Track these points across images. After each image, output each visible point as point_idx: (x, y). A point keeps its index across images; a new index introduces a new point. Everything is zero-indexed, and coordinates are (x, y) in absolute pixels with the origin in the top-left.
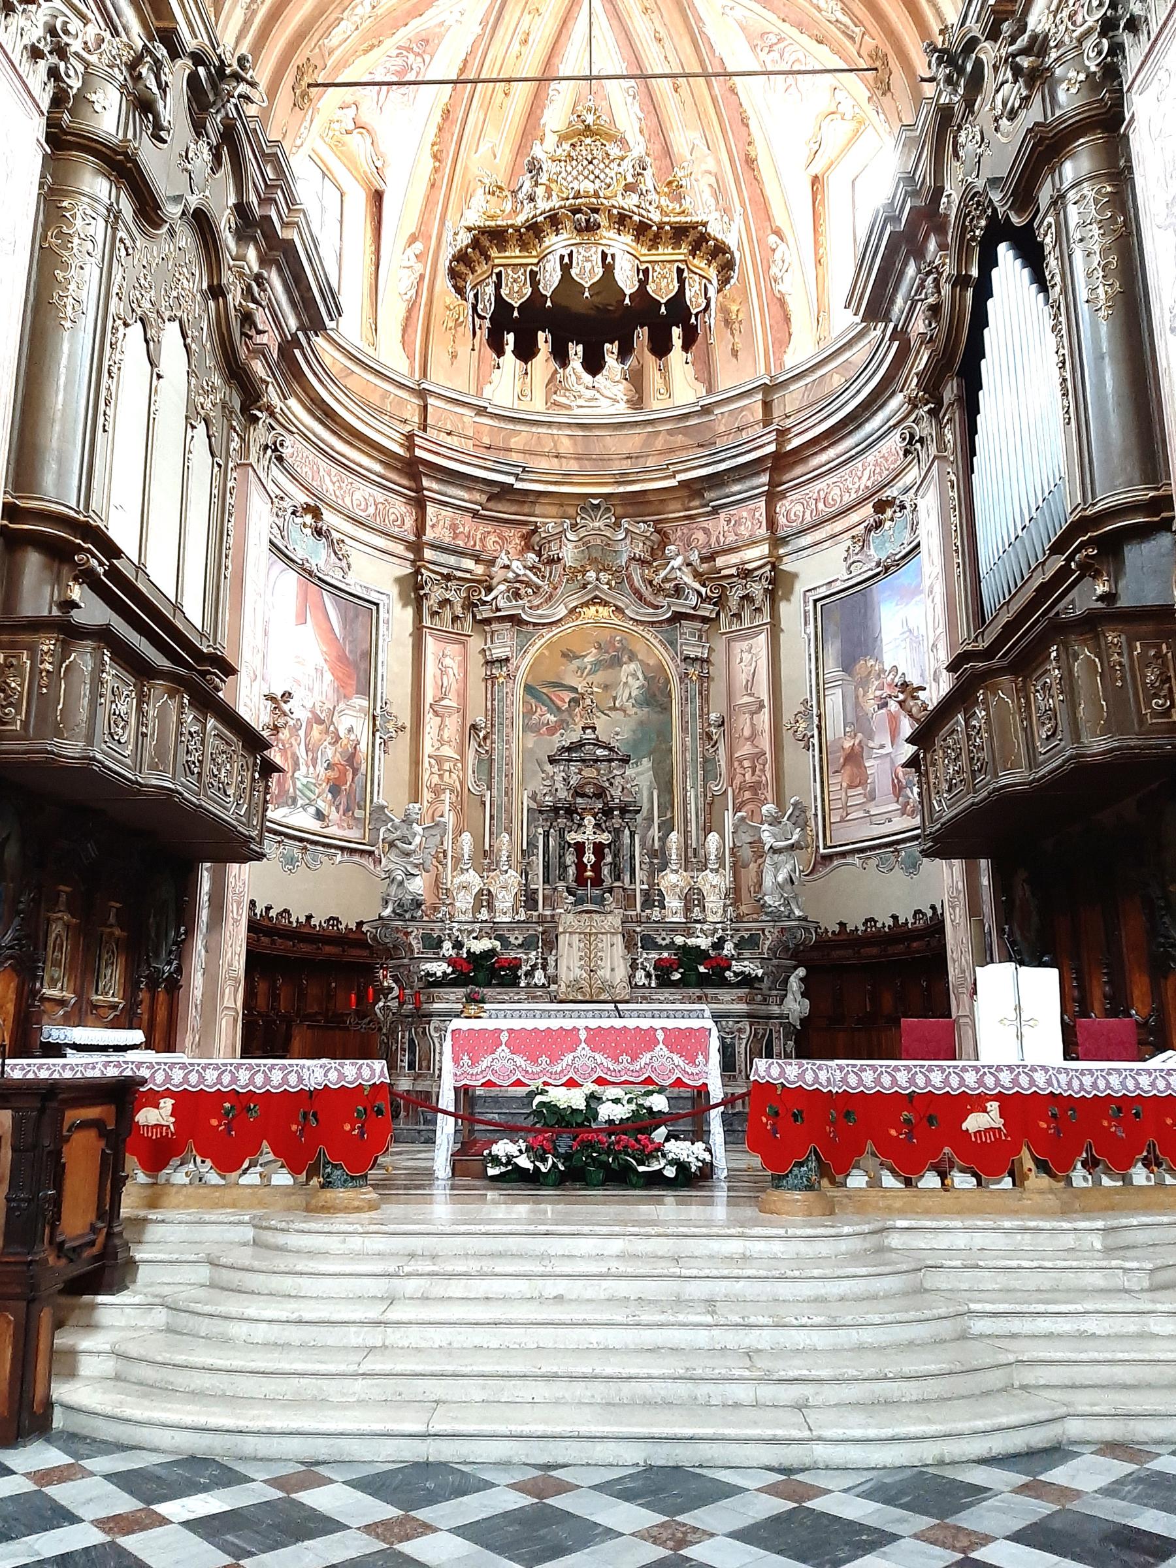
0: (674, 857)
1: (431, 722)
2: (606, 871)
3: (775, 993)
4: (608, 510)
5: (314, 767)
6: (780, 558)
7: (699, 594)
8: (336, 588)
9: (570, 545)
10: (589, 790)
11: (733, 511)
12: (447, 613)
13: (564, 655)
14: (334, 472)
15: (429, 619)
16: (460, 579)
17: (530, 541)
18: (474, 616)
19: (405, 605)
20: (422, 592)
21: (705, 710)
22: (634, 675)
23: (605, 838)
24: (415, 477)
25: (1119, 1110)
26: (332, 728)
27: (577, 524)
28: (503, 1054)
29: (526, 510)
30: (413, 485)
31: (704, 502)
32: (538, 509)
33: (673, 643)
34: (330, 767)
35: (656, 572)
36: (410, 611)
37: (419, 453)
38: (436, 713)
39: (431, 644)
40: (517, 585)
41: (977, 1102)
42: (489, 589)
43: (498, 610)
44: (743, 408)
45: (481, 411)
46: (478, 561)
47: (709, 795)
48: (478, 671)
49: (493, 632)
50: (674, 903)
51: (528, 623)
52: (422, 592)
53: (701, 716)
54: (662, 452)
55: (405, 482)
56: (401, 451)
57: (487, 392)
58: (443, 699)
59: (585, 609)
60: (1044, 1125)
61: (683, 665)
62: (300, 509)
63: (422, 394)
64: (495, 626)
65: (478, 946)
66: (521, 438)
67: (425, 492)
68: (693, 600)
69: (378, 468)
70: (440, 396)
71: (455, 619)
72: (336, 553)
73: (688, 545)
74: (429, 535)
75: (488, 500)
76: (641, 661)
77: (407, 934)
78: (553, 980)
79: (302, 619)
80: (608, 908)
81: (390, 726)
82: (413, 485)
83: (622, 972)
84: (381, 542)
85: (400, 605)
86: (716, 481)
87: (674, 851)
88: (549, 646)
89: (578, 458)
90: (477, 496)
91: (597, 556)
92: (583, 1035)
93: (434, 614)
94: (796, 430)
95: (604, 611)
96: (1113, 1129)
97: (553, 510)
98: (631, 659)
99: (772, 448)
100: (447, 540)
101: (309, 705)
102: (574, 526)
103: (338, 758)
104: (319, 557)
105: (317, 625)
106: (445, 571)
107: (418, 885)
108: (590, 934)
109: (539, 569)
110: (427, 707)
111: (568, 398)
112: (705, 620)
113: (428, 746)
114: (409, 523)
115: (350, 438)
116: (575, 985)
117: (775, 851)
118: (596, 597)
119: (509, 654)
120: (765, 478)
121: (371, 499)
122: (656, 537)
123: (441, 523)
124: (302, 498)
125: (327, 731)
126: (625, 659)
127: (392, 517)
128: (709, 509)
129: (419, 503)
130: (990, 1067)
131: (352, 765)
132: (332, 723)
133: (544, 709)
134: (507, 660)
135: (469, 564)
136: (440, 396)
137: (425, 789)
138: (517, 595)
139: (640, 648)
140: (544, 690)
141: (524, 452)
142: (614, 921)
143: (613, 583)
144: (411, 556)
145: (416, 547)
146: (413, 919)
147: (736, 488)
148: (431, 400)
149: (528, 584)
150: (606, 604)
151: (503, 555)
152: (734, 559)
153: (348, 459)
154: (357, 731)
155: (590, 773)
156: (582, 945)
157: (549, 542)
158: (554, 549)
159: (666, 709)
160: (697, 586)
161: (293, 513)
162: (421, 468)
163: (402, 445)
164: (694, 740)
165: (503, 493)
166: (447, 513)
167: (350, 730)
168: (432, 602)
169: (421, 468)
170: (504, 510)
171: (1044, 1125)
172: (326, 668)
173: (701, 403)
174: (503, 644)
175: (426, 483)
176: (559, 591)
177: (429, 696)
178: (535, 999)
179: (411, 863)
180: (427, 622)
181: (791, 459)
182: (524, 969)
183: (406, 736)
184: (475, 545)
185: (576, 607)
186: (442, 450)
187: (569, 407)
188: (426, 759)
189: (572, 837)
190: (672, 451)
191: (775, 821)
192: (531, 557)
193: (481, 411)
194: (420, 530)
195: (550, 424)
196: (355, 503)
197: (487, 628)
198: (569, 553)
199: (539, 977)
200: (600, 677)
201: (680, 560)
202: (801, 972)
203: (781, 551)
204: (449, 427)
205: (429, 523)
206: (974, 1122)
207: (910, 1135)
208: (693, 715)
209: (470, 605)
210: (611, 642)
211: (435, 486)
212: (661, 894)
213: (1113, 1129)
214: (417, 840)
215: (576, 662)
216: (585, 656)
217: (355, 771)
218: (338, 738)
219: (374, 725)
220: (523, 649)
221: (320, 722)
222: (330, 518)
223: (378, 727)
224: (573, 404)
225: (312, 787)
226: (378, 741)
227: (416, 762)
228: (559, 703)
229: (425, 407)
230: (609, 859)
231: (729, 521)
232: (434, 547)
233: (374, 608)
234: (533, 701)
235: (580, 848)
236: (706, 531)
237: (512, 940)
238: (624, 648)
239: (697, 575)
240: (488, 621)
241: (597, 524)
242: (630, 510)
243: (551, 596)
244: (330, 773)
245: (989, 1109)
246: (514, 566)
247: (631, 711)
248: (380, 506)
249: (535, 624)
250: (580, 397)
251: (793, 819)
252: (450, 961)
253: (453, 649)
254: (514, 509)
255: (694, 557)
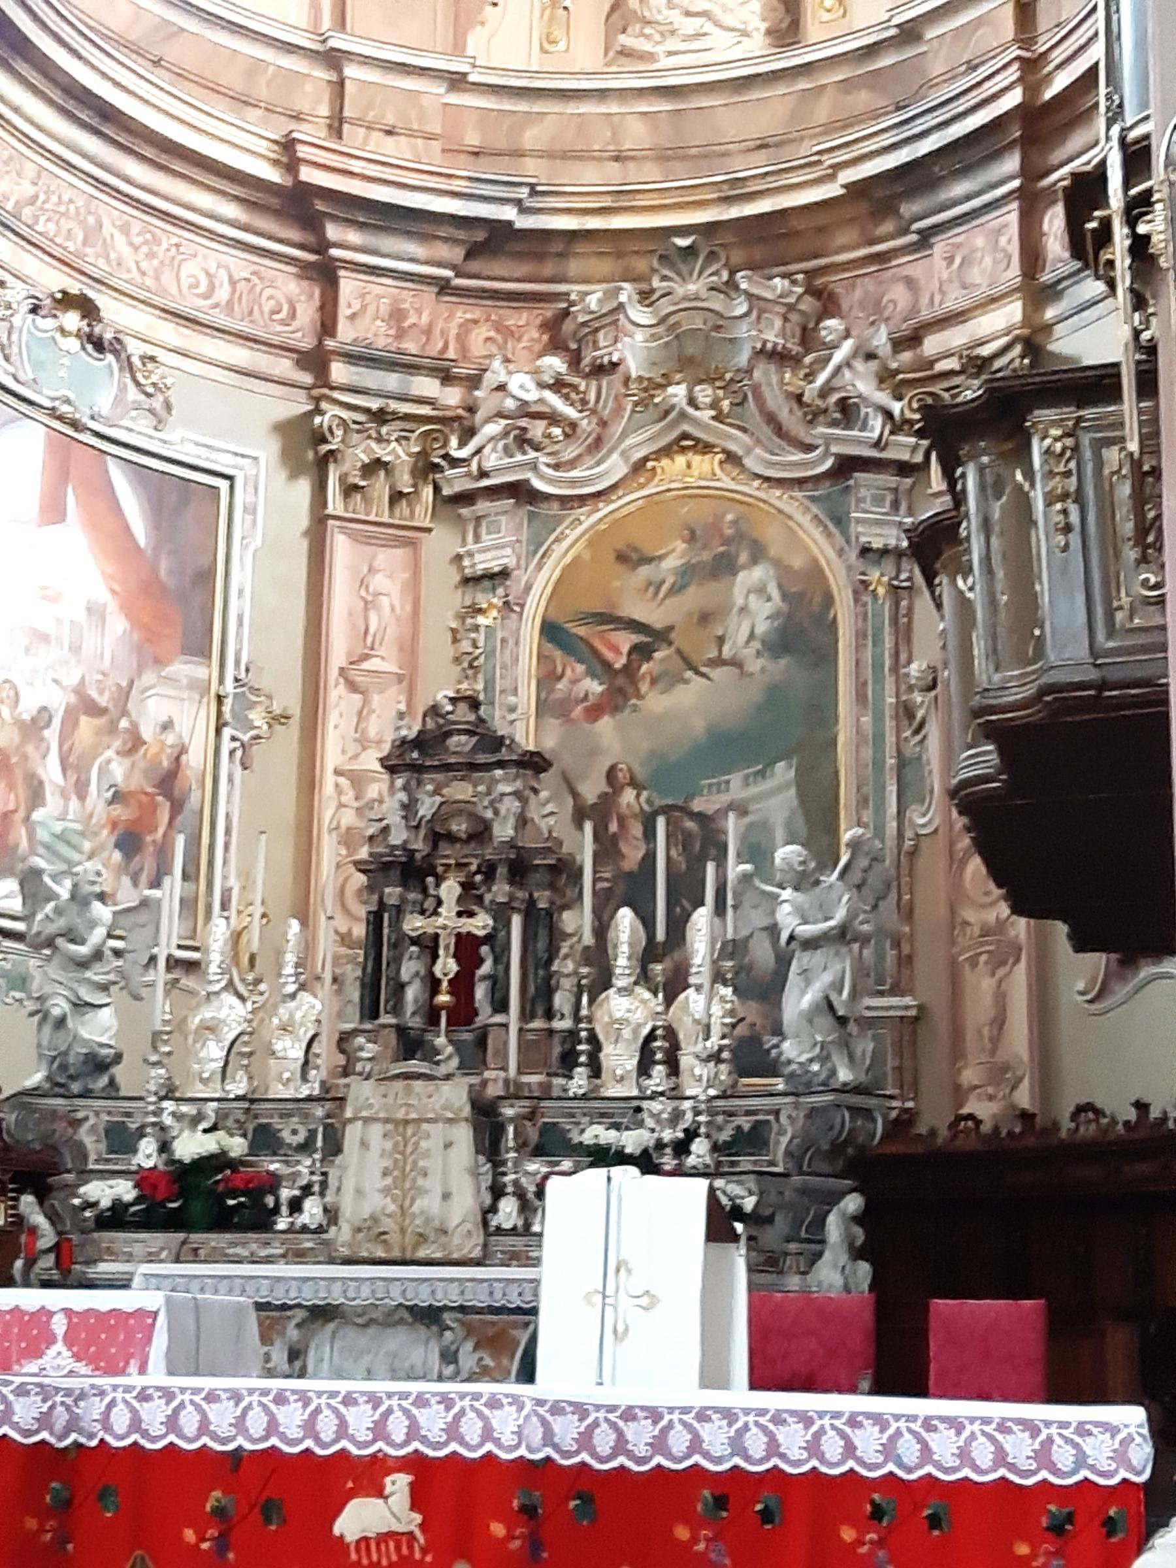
0: (622, 961)
1: (339, 706)
2: (481, 992)
3: (793, 1247)
4: (712, 256)
5: (82, 797)
6: (1048, 328)
7: (888, 415)
8: (126, 446)
9: (639, 336)
10: (459, 827)
11: (957, 235)
12: (380, 487)
13: (622, 558)
14: (136, 227)
15: (339, 498)
16: (407, 417)
17: (560, 334)
18: (437, 489)
19: (293, 475)
20: (325, 448)
21: (903, 657)
22: (761, 590)
23: (480, 924)
24: (311, 222)
25: (720, 1502)
26: (124, 723)
27: (653, 291)
28: (59, 1361)
29: (548, 269)
30: (311, 239)
31: (904, 224)
32: (574, 267)
33: (840, 521)
34: (118, 797)
35: (810, 377)
36: (303, 487)
37: (307, 175)
38: (353, 687)
39: (341, 547)
40: (523, 422)
41: (366, 1475)
42: (468, 433)
43: (483, 474)
44: (979, 21)
45: (457, 81)
46: (447, 378)
47: (909, 834)
48: (444, 601)
49: (478, 519)
50: (620, 1058)
51: (548, 497)
52: (325, 448)
53: (895, 669)
54: (829, 128)
55: (294, 235)
56: (273, 175)
57: (475, 42)
58: (365, 657)
59: (665, 462)
60: (498, 1529)
61: (859, 565)
62: (48, 302)
63: (333, 59)
64: (482, 506)
65: (191, 1145)
66: (545, 126)
67: (334, 252)
68: (877, 424)
69: (231, 210)
70: (368, 61)
71: (396, 497)
72: (138, 384)
73: (877, 310)
74: (346, 333)
75: (469, 255)
76: (777, 563)
77: (77, 1123)
78: (332, 1214)
79: (53, 511)
80: (443, 1070)
81: (257, 717)
82: (311, 239)
83: (465, 1201)
84: (240, 355)
85: (282, 475)
86: (916, 177)
87: (625, 948)
88: (595, 540)
89: (664, 156)
90: (444, 251)
91: (691, 353)
92: (59, 1325)
93: (349, 490)
94: (1058, 56)
95: (703, 464)
96: (701, 1546)
97: (605, 266)
98: (758, 554)
99: (1014, 98)
100: (381, 342)
101: (72, 680)
102: (646, 297)
103: (137, 782)
104: (100, 392)
105: (92, 523)
106: (374, 404)
107: (100, 1029)
108: (406, 1122)
109: (574, 387)
110: (334, 673)
111: (647, 37)
112: (903, 468)
113: (333, 753)
114: (308, 313)
115: (163, 159)
116: (371, 1228)
117: (811, 944)
118: (685, 436)
119: (511, 562)
120: (1012, 163)
121: (223, 275)
122: (809, 304)
123: (371, 309)
124: (55, 280)
125: (112, 729)
126: (743, 558)
127: (268, 306)
128: (914, 237)
129: (324, 273)
130: (685, 1410)
131: (169, 796)
132: (125, 713)
133: (580, 668)
134: (504, 574)
135: (427, 386)
136: (368, 61)
137: (326, 838)
138: (523, 441)
139: (773, 536)
140: (581, 631)
141: (549, 155)
142: (454, 1095)
143: (725, 405)
144: (307, 379)
145: (315, 361)
146: (86, 1094)
147: (960, 188)
148: (350, 71)
149: (553, 418)
150: (705, 448)
151: (497, 364)
152: (956, 337)
153: (166, 198)
154: (183, 726)
155: (461, 791)
156: (389, 1145)
157: (597, 330)
158: (604, 349)
159: (825, 658)
160: (883, 397)
161: (34, 310)
162: (320, 206)
163: (276, 162)
164: (878, 719)
165: (491, 240)
166: (384, 289)
167: (167, 726)
168: (346, 468)
169: (320, 206)
170: (504, 275)
171: (498, 1529)
172: (112, 606)
173: (895, 21)
174: (498, 542)
175: (333, 232)
176: (617, 429)
177: (338, 651)
178: (300, 1256)
179: (88, 981)
180: (335, 503)
181: (1062, 117)
182: (286, 1193)
183: (290, 735)
184: (446, 346)
185: (646, 459)
186: (357, 166)
187: (650, 57)
188: (329, 780)
189: (414, 924)
190: (847, 124)
191: (803, 881)
192: (555, 364)
193: (457, 81)
194: (327, 326)
195: (602, 94)
196: (185, 282)
197: (464, 511)
198: (633, 351)
199: (312, 1212)
200: (694, 598)
201: (847, 346)
202: (853, 1203)
203: (1050, 313)
204: (390, 119)
205: (343, 311)
206: (358, 1519)
207: (222, 1543)
208: (878, 666)
209: (425, 468)
210: (715, 527)
211: (353, 237)
212: (593, 1040)
213: (701, 1546)
214: (99, 934)
215: (644, 571)
216: (661, 558)
217: (177, 806)
218: (135, 743)
219: (219, 714)
220: (536, 546)
221: (93, 709)
222: (116, 313)
223: (227, 716)
224: (659, 49)
225: (75, 839)
226: (226, 746)
227: (309, 783)
228: (609, 655)
229: (341, 83)
230: (486, 968)
231: (950, 260)
232: (352, 358)
233: (223, 485)
234: (558, 654)
235: (429, 946)
236: (910, 282)
237: (286, 1135)
238: (740, 537)
239: (885, 377)
240: (466, 498)
241: (692, 287)
242: (758, 254)
243: (598, 442)
244: (118, 811)
245: (388, 1489)
246: (513, 387)
247: (754, 665)
248: (242, 286)
249: (564, 500)
250: (673, 32)
251: (856, 876)
252: (143, 1179)
253: (390, 558)
254: (523, 269)
255: (881, 340)
